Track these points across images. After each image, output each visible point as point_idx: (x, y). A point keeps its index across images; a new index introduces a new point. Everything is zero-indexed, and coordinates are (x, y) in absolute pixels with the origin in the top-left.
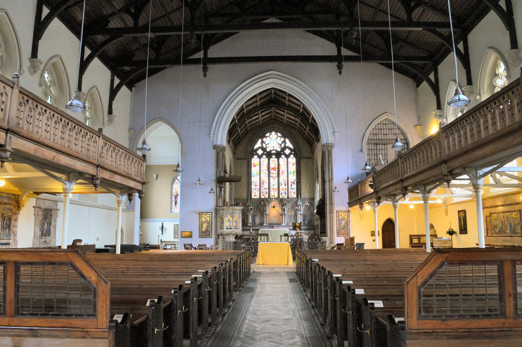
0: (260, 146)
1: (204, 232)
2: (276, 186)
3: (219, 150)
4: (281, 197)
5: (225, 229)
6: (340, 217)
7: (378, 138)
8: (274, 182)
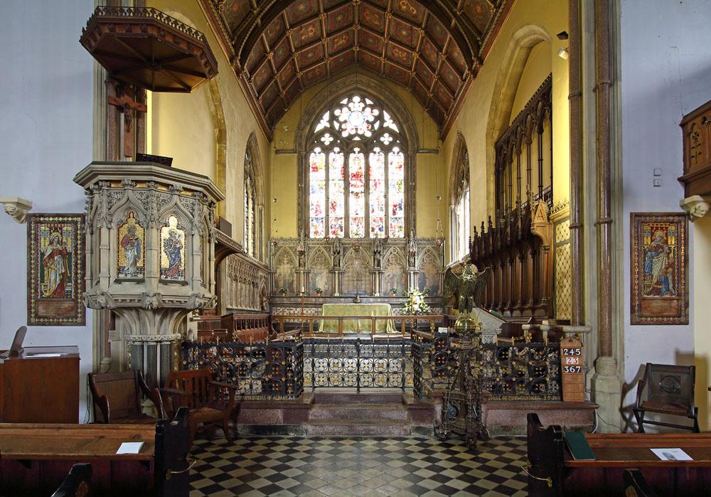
0: (328, 125)
1: (48, 300)
2: (362, 214)
4: (372, 236)
6: (647, 241)
8: (357, 205)
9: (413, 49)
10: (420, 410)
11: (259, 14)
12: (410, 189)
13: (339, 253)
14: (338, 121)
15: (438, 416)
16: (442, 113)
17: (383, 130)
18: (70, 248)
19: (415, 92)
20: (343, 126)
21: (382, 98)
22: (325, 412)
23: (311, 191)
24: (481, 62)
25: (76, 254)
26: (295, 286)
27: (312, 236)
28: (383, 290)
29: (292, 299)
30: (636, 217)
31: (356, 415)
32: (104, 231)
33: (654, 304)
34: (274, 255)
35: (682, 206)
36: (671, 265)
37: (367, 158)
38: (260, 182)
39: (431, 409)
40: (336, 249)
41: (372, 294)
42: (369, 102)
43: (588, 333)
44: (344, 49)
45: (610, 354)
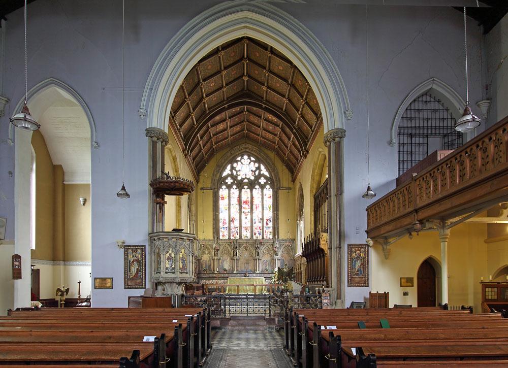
0: (230, 173)
1: (132, 279)
2: (249, 225)
3: (156, 138)
4: (255, 238)
5: (163, 274)
6: (354, 255)
7: (413, 125)
8: (246, 223)
9: (276, 135)
10: (270, 321)
11: (197, 127)
12: (276, 207)
13: (236, 248)
14: (253, 161)
15: (277, 323)
16: (293, 169)
17: (260, 176)
18: (140, 259)
19: (278, 154)
20: (238, 173)
21: (260, 157)
22: (235, 322)
23: (220, 211)
24: (308, 152)
25: (142, 261)
26: (212, 267)
27: (221, 238)
28: (260, 270)
29: (210, 275)
30: (349, 245)
31: (245, 323)
32: (162, 255)
33: (356, 279)
34: (200, 249)
35: (367, 242)
36: (362, 264)
37: (251, 192)
38: (193, 208)
39: (274, 320)
40: (235, 245)
41: (254, 272)
42: (253, 159)
43: (333, 290)
44: (238, 132)
45: (340, 299)
